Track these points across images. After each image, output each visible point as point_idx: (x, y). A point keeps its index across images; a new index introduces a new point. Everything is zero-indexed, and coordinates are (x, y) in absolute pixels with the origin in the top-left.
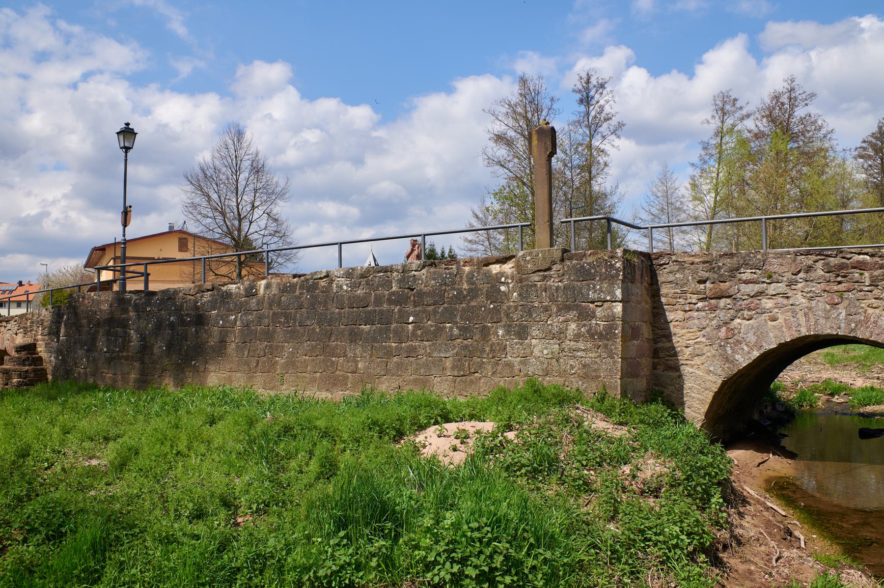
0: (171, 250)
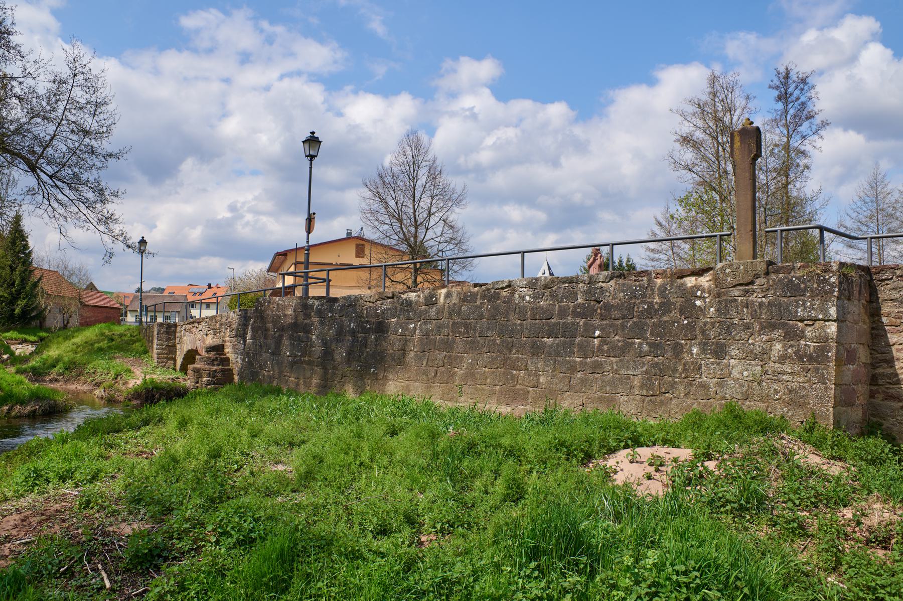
0: (349, 256)
